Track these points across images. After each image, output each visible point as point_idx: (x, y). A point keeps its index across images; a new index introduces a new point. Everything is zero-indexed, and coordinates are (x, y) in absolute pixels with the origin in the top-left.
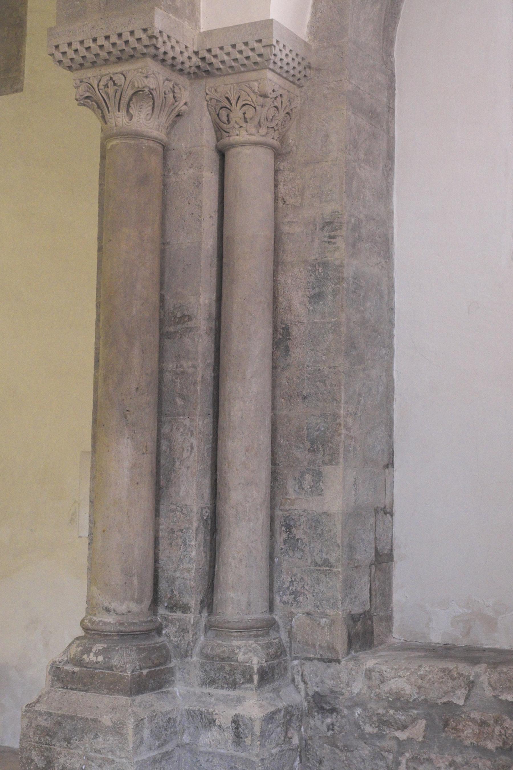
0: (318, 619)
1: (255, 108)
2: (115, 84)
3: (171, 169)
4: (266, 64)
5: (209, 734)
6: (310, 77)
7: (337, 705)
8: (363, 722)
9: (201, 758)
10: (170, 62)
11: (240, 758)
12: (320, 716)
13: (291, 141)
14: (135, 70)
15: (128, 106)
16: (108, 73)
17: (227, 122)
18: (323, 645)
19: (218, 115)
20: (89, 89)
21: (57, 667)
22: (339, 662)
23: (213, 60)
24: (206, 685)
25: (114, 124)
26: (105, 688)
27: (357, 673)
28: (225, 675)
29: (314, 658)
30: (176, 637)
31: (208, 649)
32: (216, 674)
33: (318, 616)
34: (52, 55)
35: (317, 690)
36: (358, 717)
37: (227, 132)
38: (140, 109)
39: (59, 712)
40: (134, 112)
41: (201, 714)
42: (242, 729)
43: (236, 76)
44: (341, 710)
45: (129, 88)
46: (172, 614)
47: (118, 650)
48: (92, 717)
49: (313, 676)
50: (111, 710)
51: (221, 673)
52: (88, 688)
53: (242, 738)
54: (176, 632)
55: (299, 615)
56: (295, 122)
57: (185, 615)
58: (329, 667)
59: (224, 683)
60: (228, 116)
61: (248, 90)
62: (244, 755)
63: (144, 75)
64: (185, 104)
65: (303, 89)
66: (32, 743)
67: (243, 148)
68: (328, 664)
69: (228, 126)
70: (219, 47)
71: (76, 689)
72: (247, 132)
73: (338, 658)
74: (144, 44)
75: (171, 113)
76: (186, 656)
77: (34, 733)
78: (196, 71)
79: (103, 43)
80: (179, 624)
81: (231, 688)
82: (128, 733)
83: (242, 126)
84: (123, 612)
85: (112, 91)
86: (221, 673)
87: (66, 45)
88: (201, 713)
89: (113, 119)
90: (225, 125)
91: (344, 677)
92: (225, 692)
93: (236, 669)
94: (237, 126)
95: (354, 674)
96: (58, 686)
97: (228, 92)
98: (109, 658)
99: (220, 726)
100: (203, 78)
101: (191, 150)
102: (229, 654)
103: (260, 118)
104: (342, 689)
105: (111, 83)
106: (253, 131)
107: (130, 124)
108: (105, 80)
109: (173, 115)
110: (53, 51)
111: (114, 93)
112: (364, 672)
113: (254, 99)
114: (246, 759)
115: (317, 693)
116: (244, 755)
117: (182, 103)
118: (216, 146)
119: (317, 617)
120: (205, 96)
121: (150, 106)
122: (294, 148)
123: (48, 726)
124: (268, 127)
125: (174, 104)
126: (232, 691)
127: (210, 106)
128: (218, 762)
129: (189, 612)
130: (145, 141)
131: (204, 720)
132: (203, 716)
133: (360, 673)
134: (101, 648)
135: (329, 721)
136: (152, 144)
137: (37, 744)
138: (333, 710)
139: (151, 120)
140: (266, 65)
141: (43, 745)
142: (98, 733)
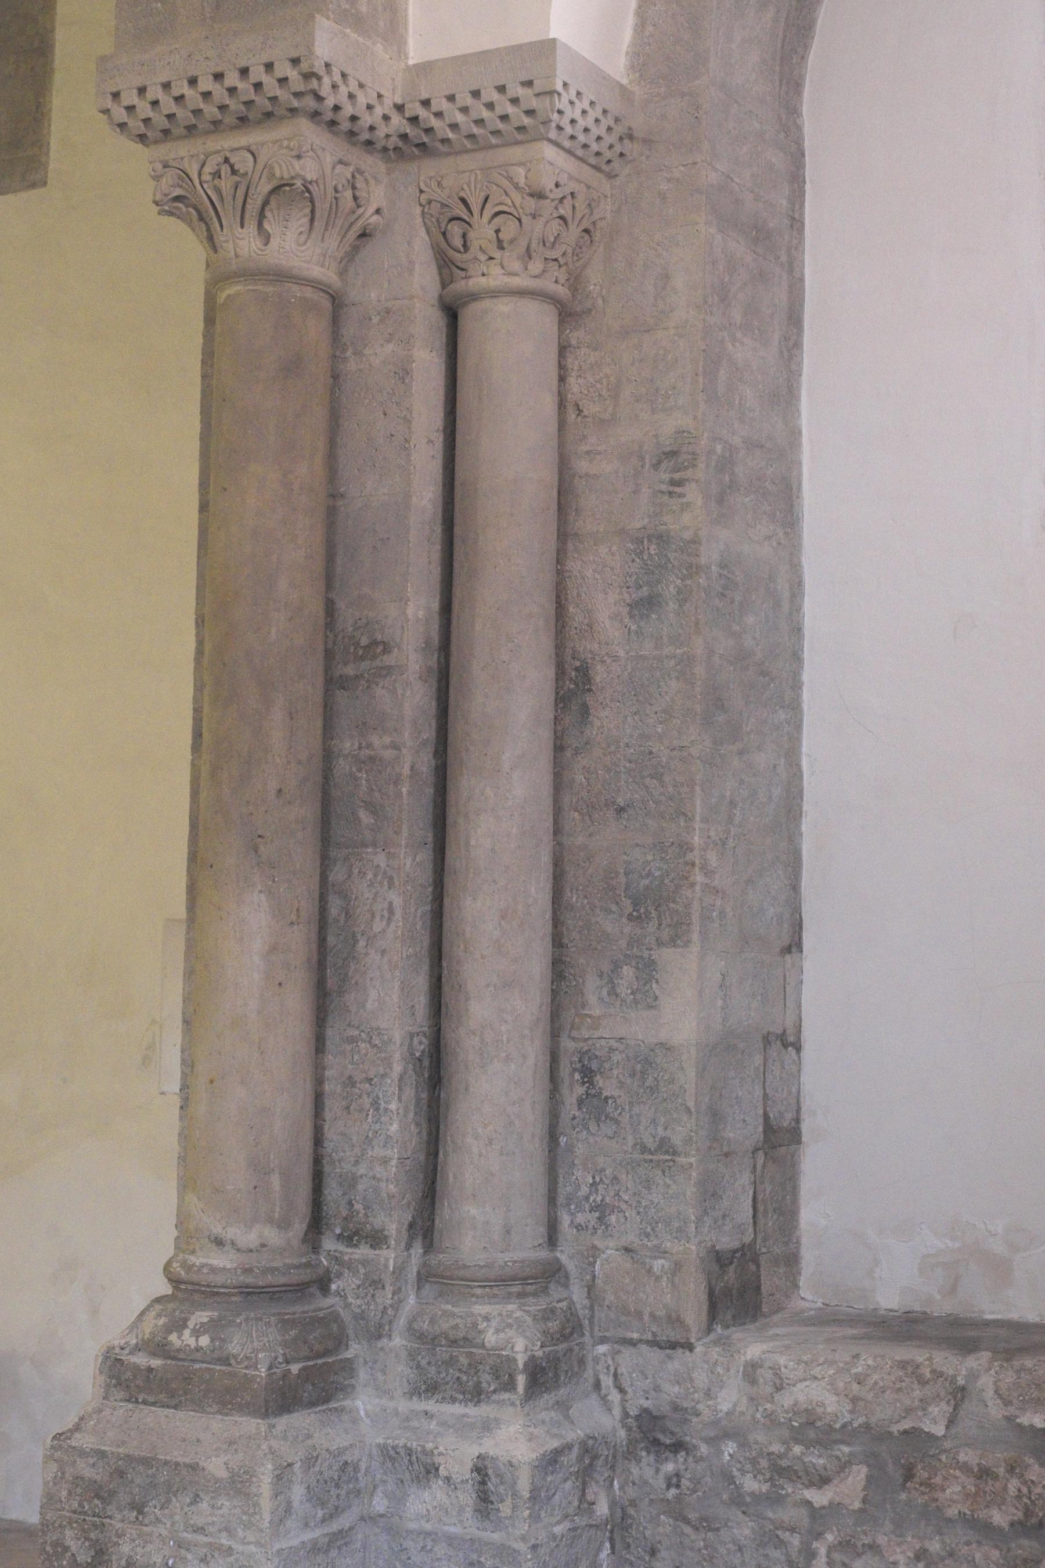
0: (647, 1260)
1: (520, 220)
2: (234, 172)
3: (348, 343)
4: (542, 130)
5: (426, 1495)
6: (631, 158)
7: (686, 1435)
8: (738, 1470)
9: (409, 1544)
10: (346, 125)
11: (489, 1544)
12: (652, 1458)
13: (592, 287)
14: (275, 142)
15: (262, 216)
16: (219, 148)
17: (462, 249)
18: (658, 1313)
19: (444, 234)
20: (180, 182)
21: (116, 1359)
22: (691, 1348)
23: (434, 123)
24: (420, 1394)
25: (233, 253)
26: (213, 1401)
27: (728, 1370)
28: (457, 1374)
29: (641, 1341)
30: (358, 1298)
31: (424, 1322)
32: (439, 1373)
33: (648, 1254)
34: (106, 111)
35: (645, 1406)
36: (728, 1461)
37: (462, 269)
38: (285, 222)
39: (120, 1450)
40: (272, 229)
41: (409, 1455)
42: (493, 1485)
43: (480, 155)
44: (695, 1447)
45: (262, 180)
46: (350, 1250)
47: (241, 1323)
48: (187, 1460)
49: (637, 1376)
50: (225, 1447)
51: (451, 1371)
52: (180, 1401)
53: (492, 1503)
54: (359, 1287)
55: (609, 1252)
56: (601, 249)
57: (377, 1252)
58: (670, 1357)
59: (455, 1390)
60: (464, 236)
61: (505, 183)
62: (496, 1537)
63: (294, 153)
64: (378, 211)
65: (617, 182)
66: (65, 1513)
67: (495, 300)
68: (668, 1351)
69: (464, 256)
70: (445, 96)
71: (156, 1402)
72: (503, 268)
73: (688, 1339)
74: (293, 90)
75: (348, 230)
76: (380, 1337)
77: (70, 1493)
78: (400, 144)
79: (210, 88)
80: (364, 1271)
81: (471, 1401)
82: (261, 1494)
83: (493, 256)
84: (251, 1246)
85: (229, 184)
86: (451, 1371)
87: (135, 91)
88: (409, 1452)
89: (231, 242)
90: (458, 255)
91: (701, 1379)
92: (458, 1409)
93: (481, 1363)
94: (483, 257)
95: (721, 1372)
96: (118, 1397)
97: (465, 186)
98: (223, 1340)
99: (448, 1479)
100: (413, 158)
101: (389, 304)
102: (466, 1332)
103: (530, 240)
104: (697, 1403)
105: (225, 170)
106: (516, 266)
107: (264, 253)
108: (215, 162)
109: (352, 234)
110: (109, 103)
111: (233, 190)
112: (741, 1369)
113: (518, 201)
114: (501, 1545)
115: (646, 1411)
116: (496, 1537)
117: (371, 210)
118: (441, 298)
119: (646, 1256)
120: (418, 195)
121: (305, 216)
122: (600, 301)
123: (98, 1478)
124: (546, 259)
125: (354, 212)
126: (473, 1408)
127: (429, 216)
128: (443, 1552)
129: (385, 1247)
130: (295, 288)
131: (416, 1466)
132: (414, 1458)
133: (733, 1371)
134: (205, 1320)
135: (670, 1467)
136: (309, 293)
137: (75, 1516)
138: (678, 1447)
139: (308, 244)
140: (542, 133)
141: (87, 1518)
142: (200, 1493)
